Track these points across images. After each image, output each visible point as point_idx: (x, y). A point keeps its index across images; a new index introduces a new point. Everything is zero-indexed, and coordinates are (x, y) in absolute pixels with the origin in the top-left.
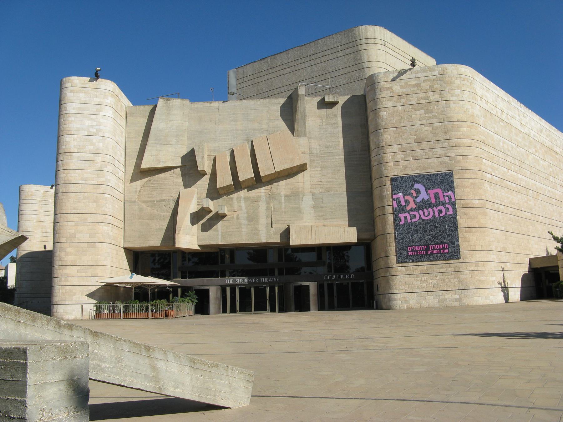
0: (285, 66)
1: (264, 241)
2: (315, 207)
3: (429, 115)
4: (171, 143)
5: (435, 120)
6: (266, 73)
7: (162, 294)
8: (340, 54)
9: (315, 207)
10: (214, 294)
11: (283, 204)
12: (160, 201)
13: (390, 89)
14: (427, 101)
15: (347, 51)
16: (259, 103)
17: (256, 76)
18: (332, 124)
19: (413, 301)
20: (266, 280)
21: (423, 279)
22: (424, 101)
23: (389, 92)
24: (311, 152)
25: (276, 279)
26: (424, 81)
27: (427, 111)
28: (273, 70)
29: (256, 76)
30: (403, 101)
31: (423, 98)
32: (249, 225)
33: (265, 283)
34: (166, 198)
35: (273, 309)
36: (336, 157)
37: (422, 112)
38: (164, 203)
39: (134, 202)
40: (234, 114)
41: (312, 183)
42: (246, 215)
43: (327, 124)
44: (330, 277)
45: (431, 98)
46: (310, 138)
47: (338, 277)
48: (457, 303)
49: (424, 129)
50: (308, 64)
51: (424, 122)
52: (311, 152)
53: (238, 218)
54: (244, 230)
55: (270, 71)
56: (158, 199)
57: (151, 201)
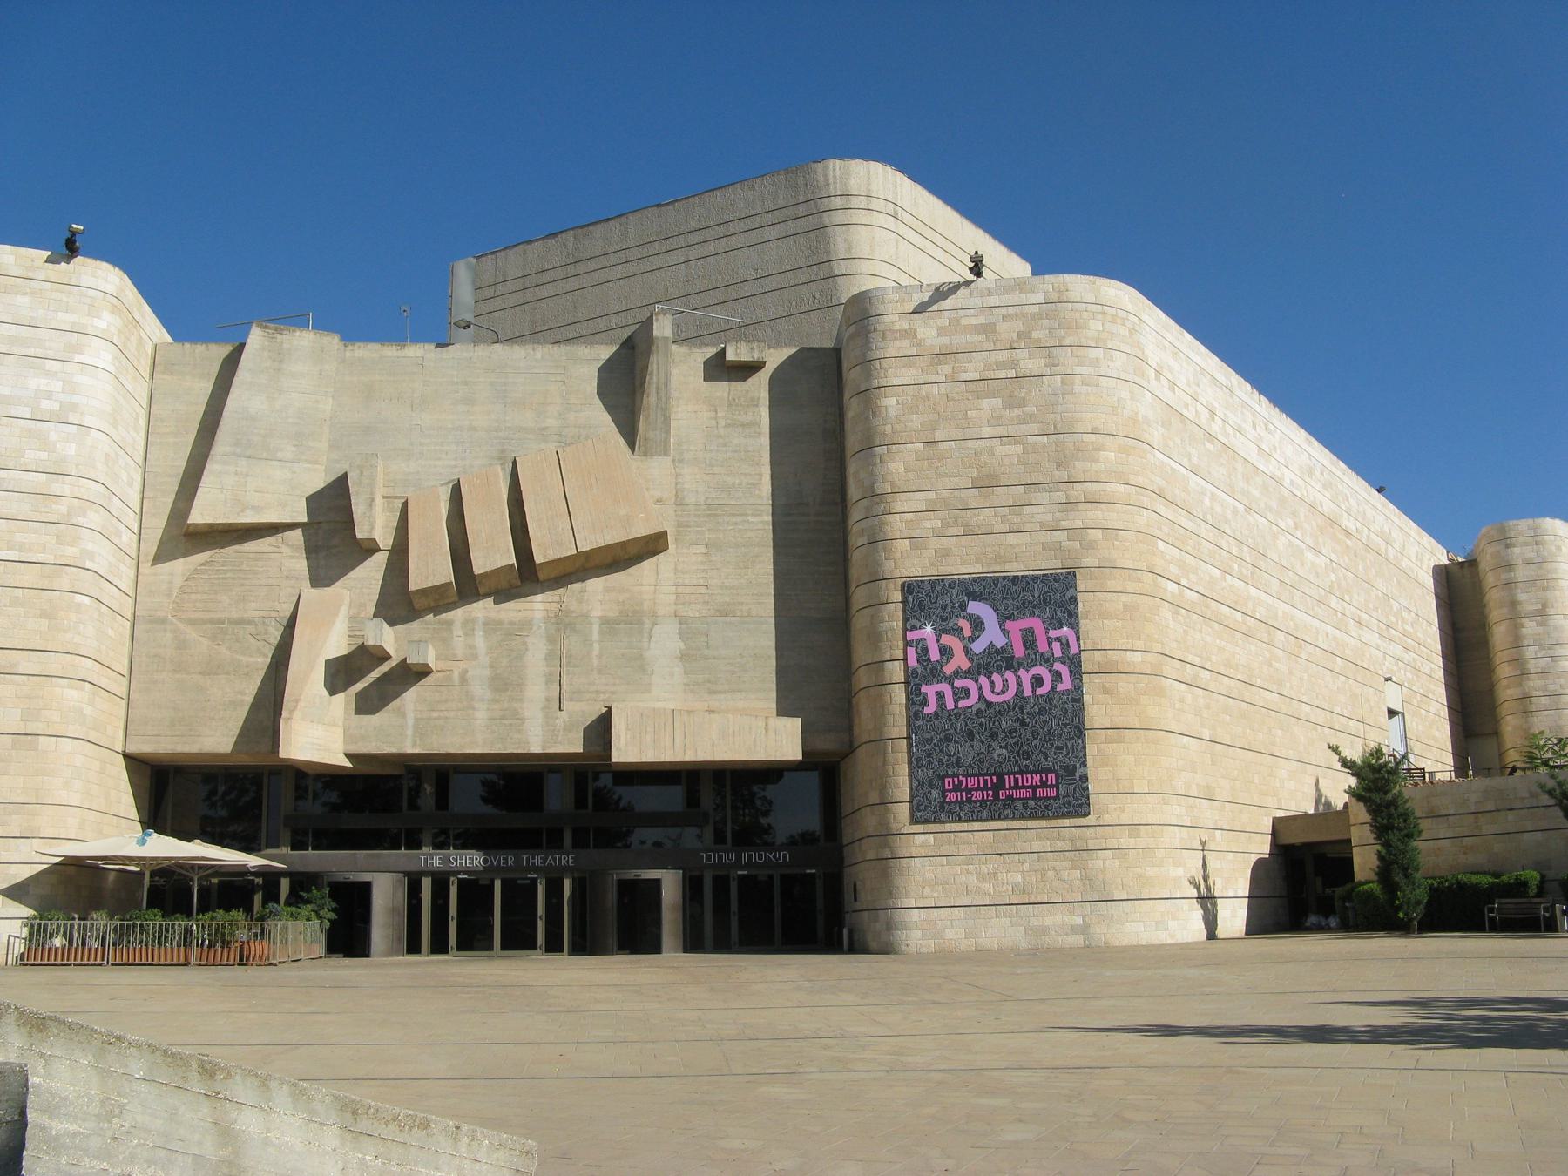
0: (613, 259)
1: (536, 748)
2: (684, 657)
3: (1016, 411)
4: (280, 455)
5: (1032, 428)
6: (560, 273)
7: (232, 892)
8: (770, 233)
9: (684, 657)
10: (385, 895)
11: (596, 646)
12: (240, 622)
13: (909, 334)
14: (1012, 374)
15: (791, 227)
16: (539, 355)
17: (530, 282)
18: (743, 425)
19: (955, 932)
20: (538, 860)
21: (984, 869)
22: (1002, 374)
23: (906, 343)
24: (679, 503)
25: (567, 860)
26: (1005, 318)
27: (1011, 402)
28: (581, 268)
29: (530, 282)
30: (945, 369)
31: (999, 366)
32: (495, 701)
33: (536, 869)
34: (256, 614)
35: (554, 946)
36: (751, 519)
37: (997, 402)
38: (251, 629)
39: (163, 621)
40: (466, 383)
41: (680, 589)
42: (487, 672)
43: (727, 426)
44: (720, 858)
45: (1022, 364)
46: (681, 461)
47: (744, 858)
48: (1077, 940)
49: (1001, 450)
50: (679, 257)
51: (1000, 431)
52: (679, 503)
53: (464, 680)
54: (481, 715)
55: (571, 270)
56: (235, 615)
57: (211, 621)
